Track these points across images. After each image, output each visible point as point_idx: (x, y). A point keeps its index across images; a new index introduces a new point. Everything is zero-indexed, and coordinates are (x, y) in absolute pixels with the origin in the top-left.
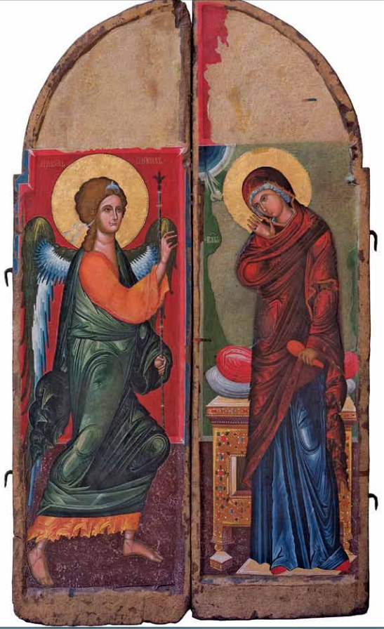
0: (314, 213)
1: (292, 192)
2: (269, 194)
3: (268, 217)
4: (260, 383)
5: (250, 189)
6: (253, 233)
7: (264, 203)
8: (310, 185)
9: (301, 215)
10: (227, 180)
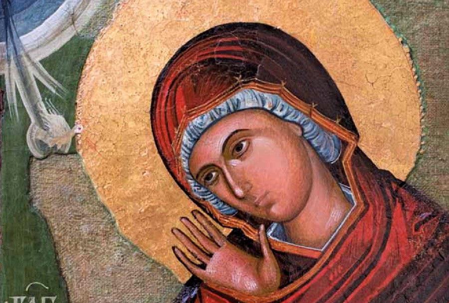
0: (430, 203)
1: (348, 123)
2: (259, 132)
3: (255, 222)
4: (187, 105)
5: (182, 109)
6: (194, 281)
7: (235, 162)
8: (415, 94)
9: (381, 215)
10: (92, 76)
